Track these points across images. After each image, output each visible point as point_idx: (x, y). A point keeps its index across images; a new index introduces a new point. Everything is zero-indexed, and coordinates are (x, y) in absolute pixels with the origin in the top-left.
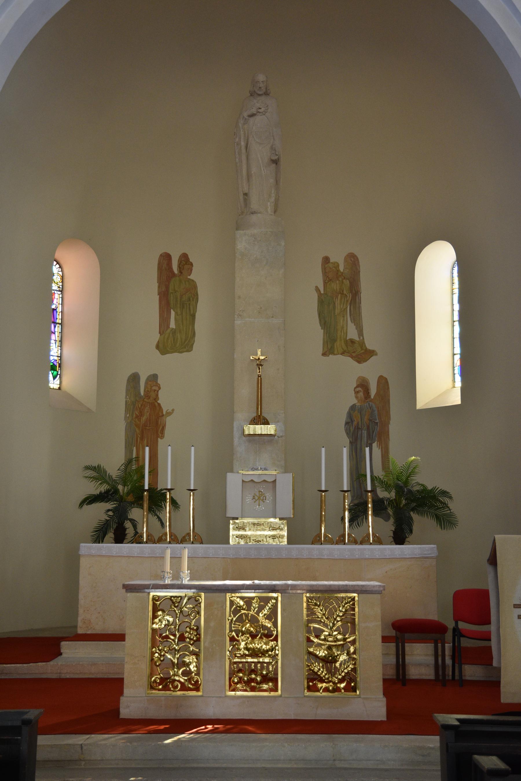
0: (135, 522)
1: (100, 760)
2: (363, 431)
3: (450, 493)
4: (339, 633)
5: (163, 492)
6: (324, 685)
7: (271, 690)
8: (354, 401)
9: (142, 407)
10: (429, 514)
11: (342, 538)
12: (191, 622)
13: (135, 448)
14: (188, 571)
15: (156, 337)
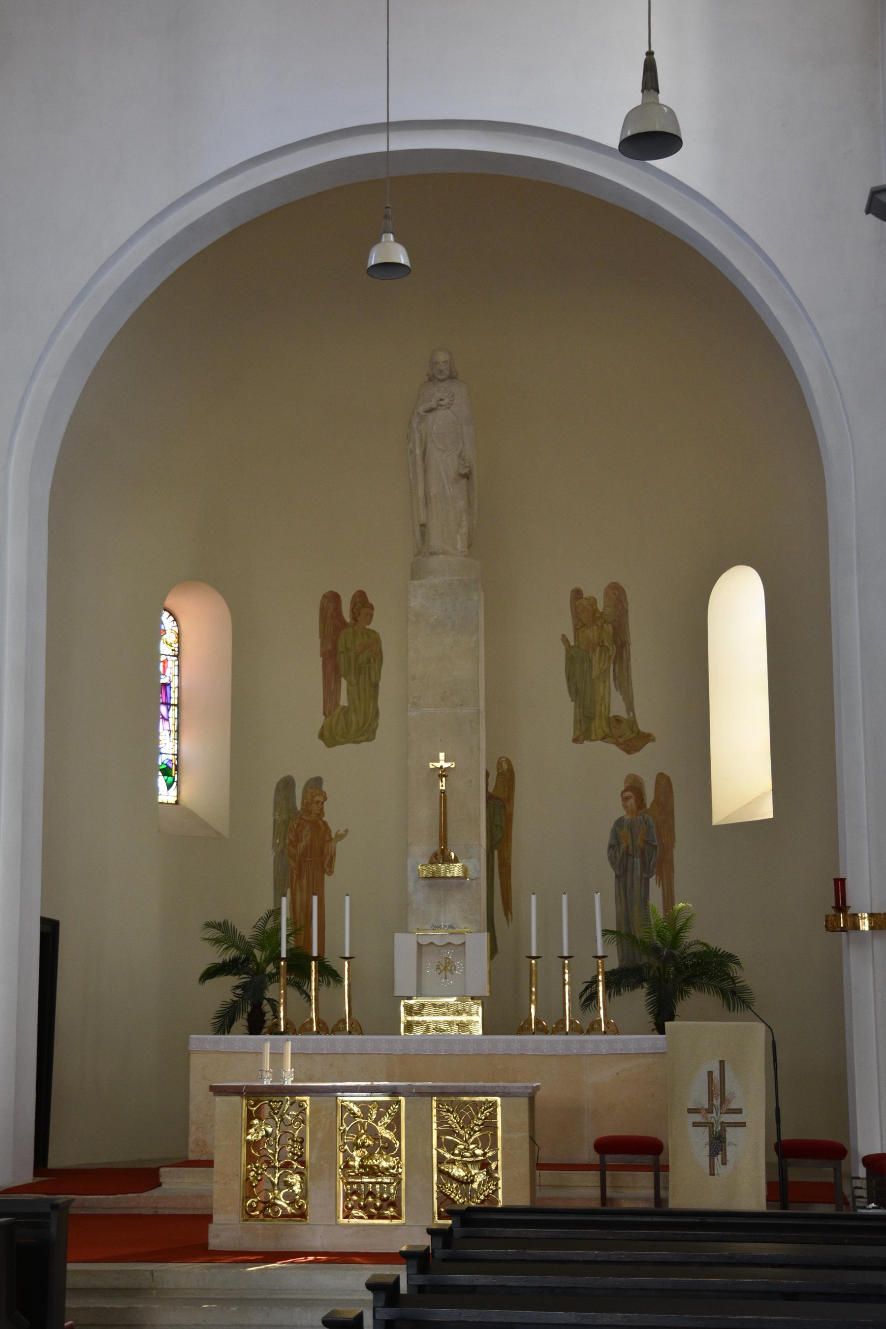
0: (275, 1003)
1: (173, 1289)
2: (635, 859)
3: (736, 957)
7: (393, 1217)
8: (621, 812)
9: (299, 829)
10: (711, 989)
11: (561, 1026)
12: (295, 1133)
14: (291, 1069)
15: (319, 720)
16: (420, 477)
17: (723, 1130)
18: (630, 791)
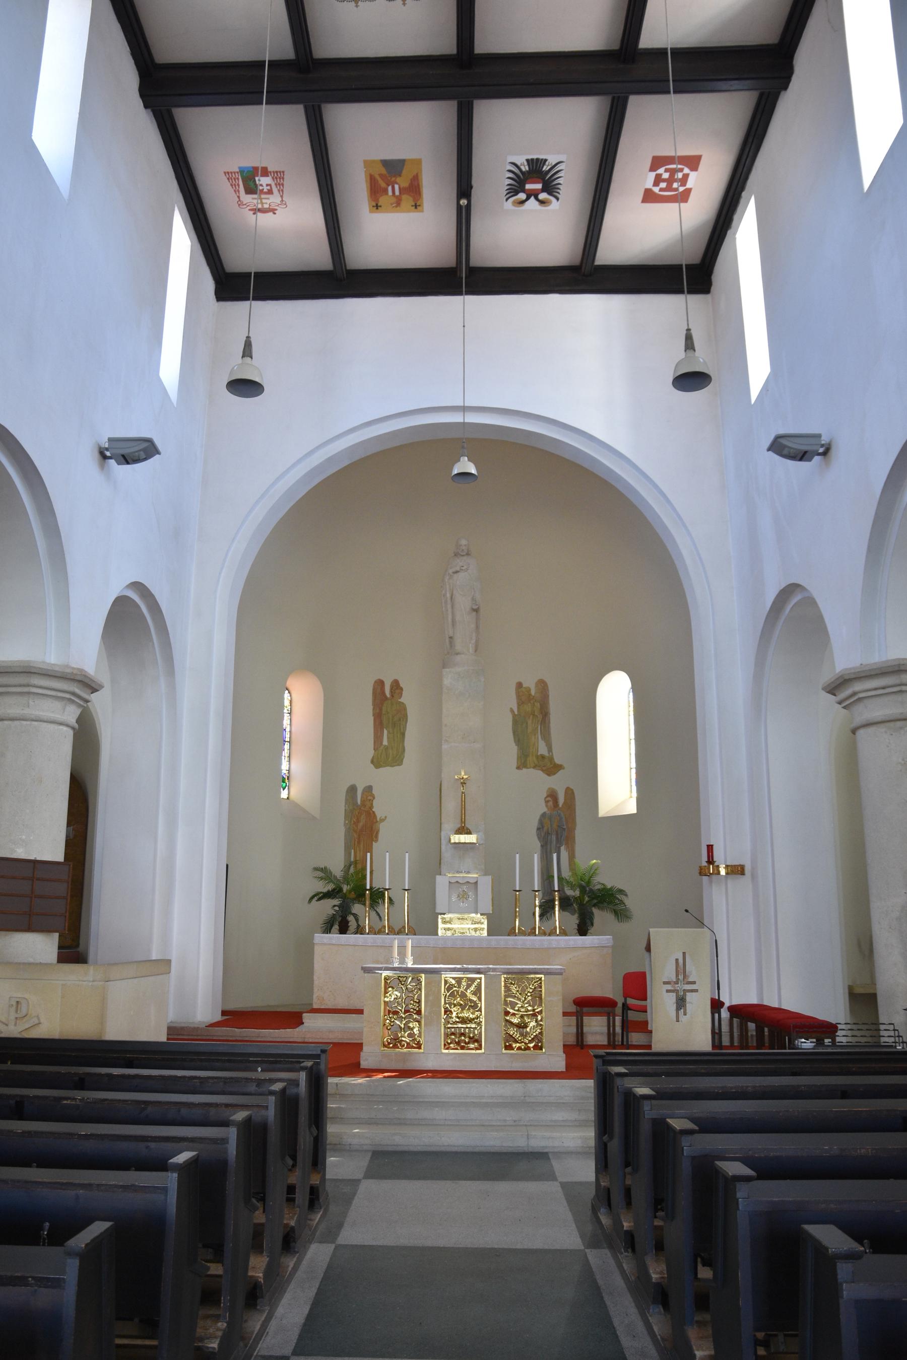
4: (530, 1005)
5: (380, 890)
6: (518, 1045)
7: (477, 1049)
8: (545, 809)
11: (513, 931)
13: (353, 851)
15: (371, 753)
16: (450, 610)
17: (685, 995)
18: (550, 797)
